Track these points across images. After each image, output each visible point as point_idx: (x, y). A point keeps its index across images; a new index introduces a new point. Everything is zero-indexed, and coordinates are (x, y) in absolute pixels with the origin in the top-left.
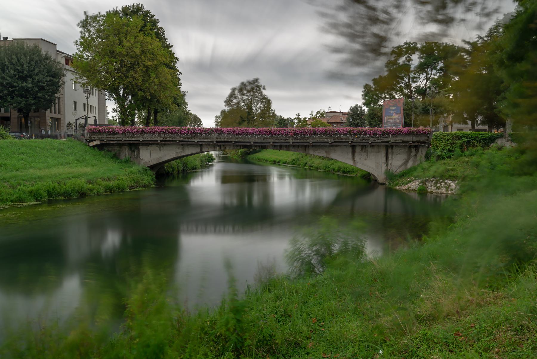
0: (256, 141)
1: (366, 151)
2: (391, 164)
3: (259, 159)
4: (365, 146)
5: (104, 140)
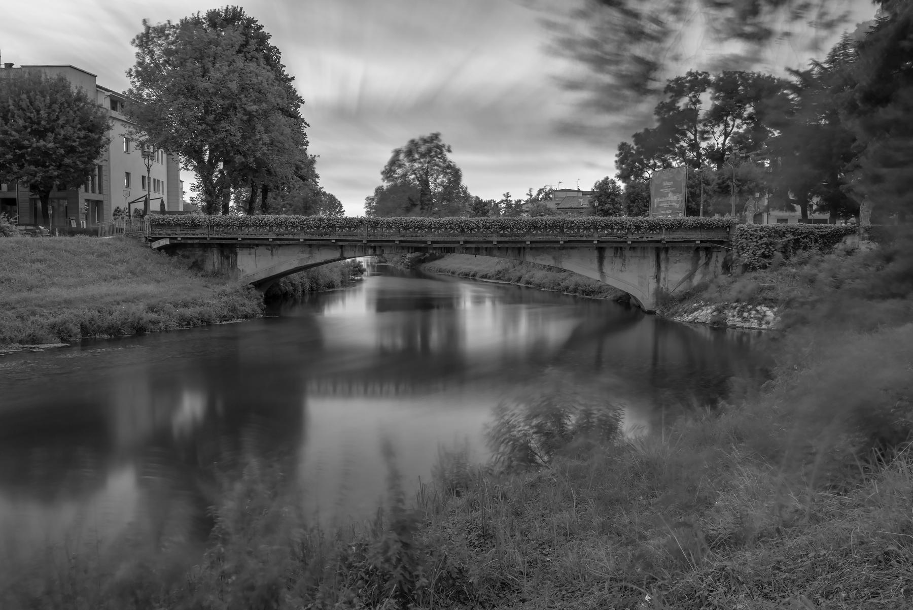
0: (435, 239)
1: (623, 257)
3: (440, 271)
4: (621, 248)
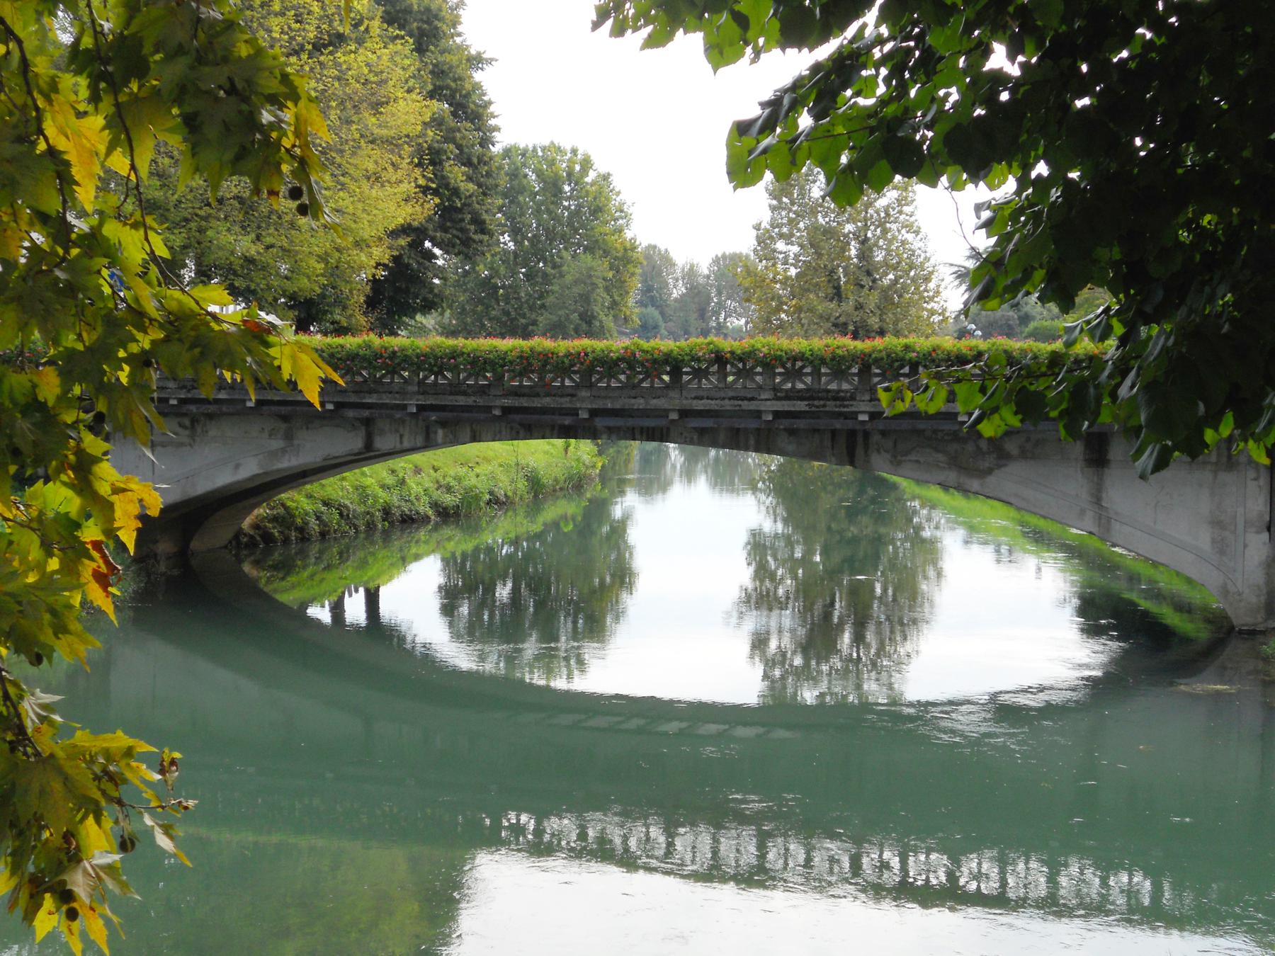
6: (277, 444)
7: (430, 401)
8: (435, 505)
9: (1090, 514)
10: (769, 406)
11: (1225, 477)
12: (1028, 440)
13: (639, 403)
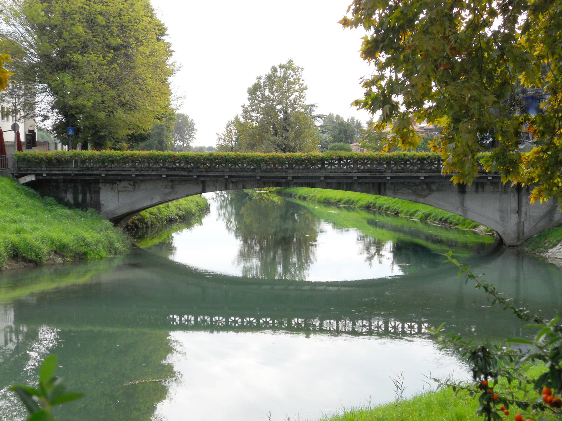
2: (526, 214)
4: (482, 183)
5: (41, 175)
6: (168, 190)
7: (234, 174)
8: (177, 215)
9: (460, 209)
10: (356, 175)
11: (504, 196)
12: (439, 185)
13: (311, 174)
